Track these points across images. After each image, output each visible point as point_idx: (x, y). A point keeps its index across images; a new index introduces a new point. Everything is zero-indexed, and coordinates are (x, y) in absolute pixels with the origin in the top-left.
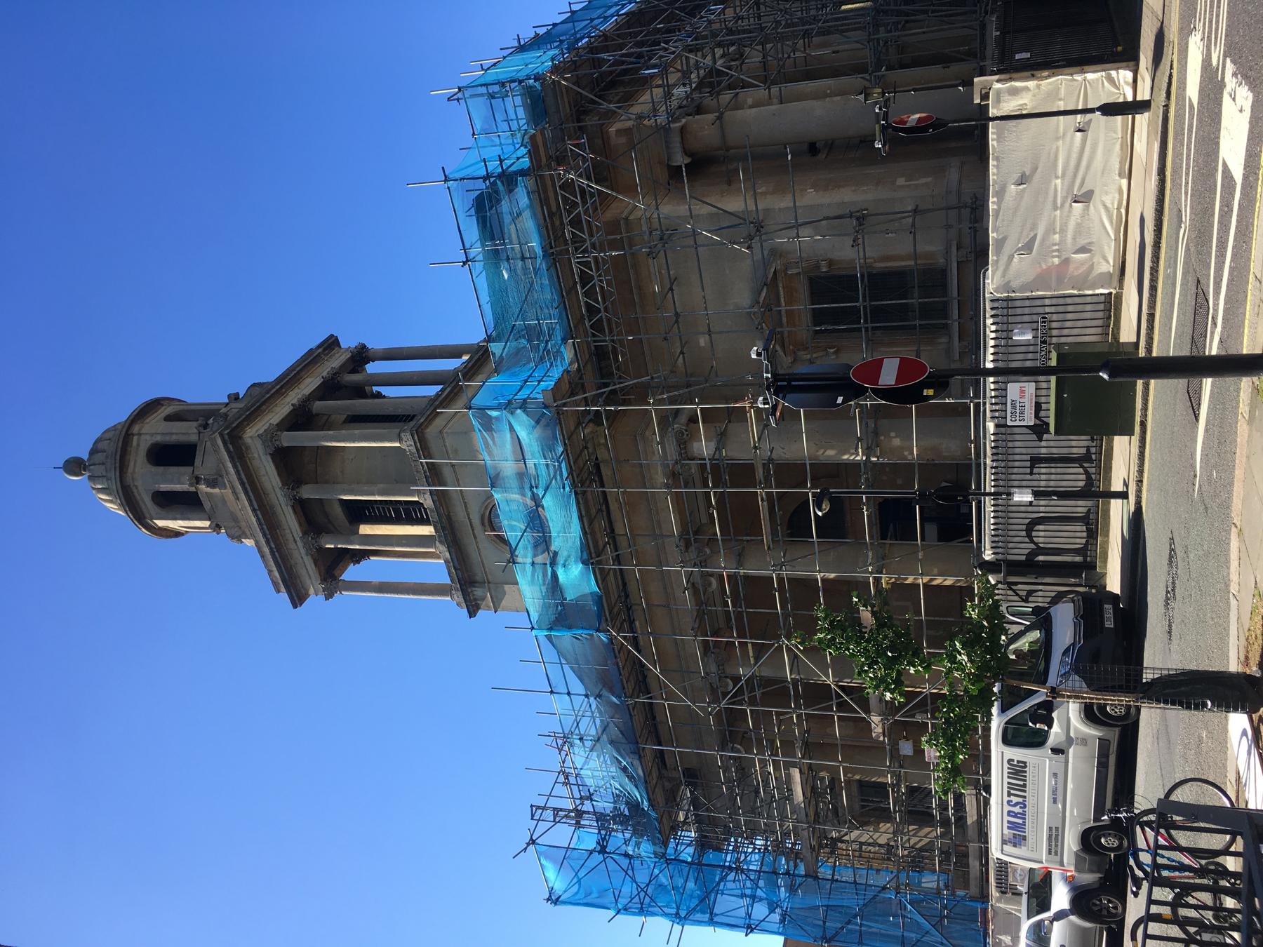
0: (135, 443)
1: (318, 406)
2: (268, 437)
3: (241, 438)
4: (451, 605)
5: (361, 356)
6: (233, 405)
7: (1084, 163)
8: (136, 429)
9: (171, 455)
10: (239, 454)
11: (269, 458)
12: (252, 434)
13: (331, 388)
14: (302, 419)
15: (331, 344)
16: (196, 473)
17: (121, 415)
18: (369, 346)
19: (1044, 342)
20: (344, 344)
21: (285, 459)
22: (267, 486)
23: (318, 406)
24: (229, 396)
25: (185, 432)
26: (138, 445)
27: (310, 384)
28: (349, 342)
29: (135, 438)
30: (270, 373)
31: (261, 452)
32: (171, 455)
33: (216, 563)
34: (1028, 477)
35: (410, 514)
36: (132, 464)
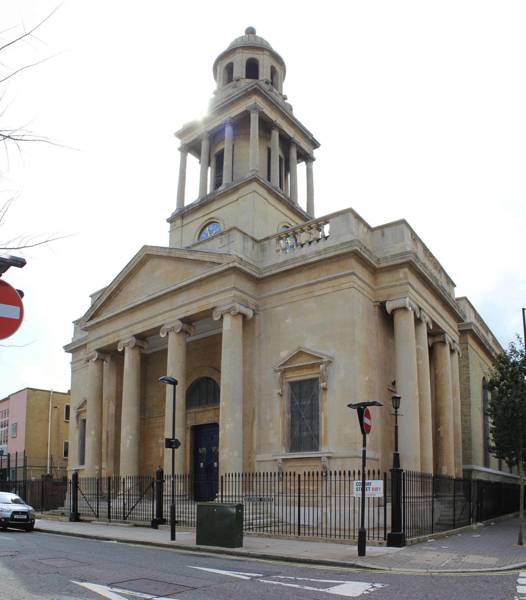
0: (259, 52)
1: (275, 134)
2: (256, 108)
3: (255, 94)
4: (172, 208)
5: (307, 158)
6: (280, 97)
7: (202, 553)
8: (267, 53)
9: (252, 70)
10: (247, 94)
11: (245, 109)
12: (255, 100)
13: (286, 142)
14: (266, 126)
15: (315, 145)
16: (242, 80)
17: (276, 48)
18: (314, 163)
19: (261, 500)
20: (315, 151)
21: (245, 117)
22: (232, 110)
23: (275, 134)
24: (285, 95)
25: (264, 74)
26: (258, 54)
27: (290, 132)
28: (316, 153)
29: (262, 53)
30: (298, 114)
31: (248, 105)
32: (252, 70)
33: (198, 99)
34: (324, 495)
35: (218, 183)
36: (247, 52)
